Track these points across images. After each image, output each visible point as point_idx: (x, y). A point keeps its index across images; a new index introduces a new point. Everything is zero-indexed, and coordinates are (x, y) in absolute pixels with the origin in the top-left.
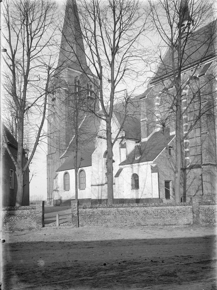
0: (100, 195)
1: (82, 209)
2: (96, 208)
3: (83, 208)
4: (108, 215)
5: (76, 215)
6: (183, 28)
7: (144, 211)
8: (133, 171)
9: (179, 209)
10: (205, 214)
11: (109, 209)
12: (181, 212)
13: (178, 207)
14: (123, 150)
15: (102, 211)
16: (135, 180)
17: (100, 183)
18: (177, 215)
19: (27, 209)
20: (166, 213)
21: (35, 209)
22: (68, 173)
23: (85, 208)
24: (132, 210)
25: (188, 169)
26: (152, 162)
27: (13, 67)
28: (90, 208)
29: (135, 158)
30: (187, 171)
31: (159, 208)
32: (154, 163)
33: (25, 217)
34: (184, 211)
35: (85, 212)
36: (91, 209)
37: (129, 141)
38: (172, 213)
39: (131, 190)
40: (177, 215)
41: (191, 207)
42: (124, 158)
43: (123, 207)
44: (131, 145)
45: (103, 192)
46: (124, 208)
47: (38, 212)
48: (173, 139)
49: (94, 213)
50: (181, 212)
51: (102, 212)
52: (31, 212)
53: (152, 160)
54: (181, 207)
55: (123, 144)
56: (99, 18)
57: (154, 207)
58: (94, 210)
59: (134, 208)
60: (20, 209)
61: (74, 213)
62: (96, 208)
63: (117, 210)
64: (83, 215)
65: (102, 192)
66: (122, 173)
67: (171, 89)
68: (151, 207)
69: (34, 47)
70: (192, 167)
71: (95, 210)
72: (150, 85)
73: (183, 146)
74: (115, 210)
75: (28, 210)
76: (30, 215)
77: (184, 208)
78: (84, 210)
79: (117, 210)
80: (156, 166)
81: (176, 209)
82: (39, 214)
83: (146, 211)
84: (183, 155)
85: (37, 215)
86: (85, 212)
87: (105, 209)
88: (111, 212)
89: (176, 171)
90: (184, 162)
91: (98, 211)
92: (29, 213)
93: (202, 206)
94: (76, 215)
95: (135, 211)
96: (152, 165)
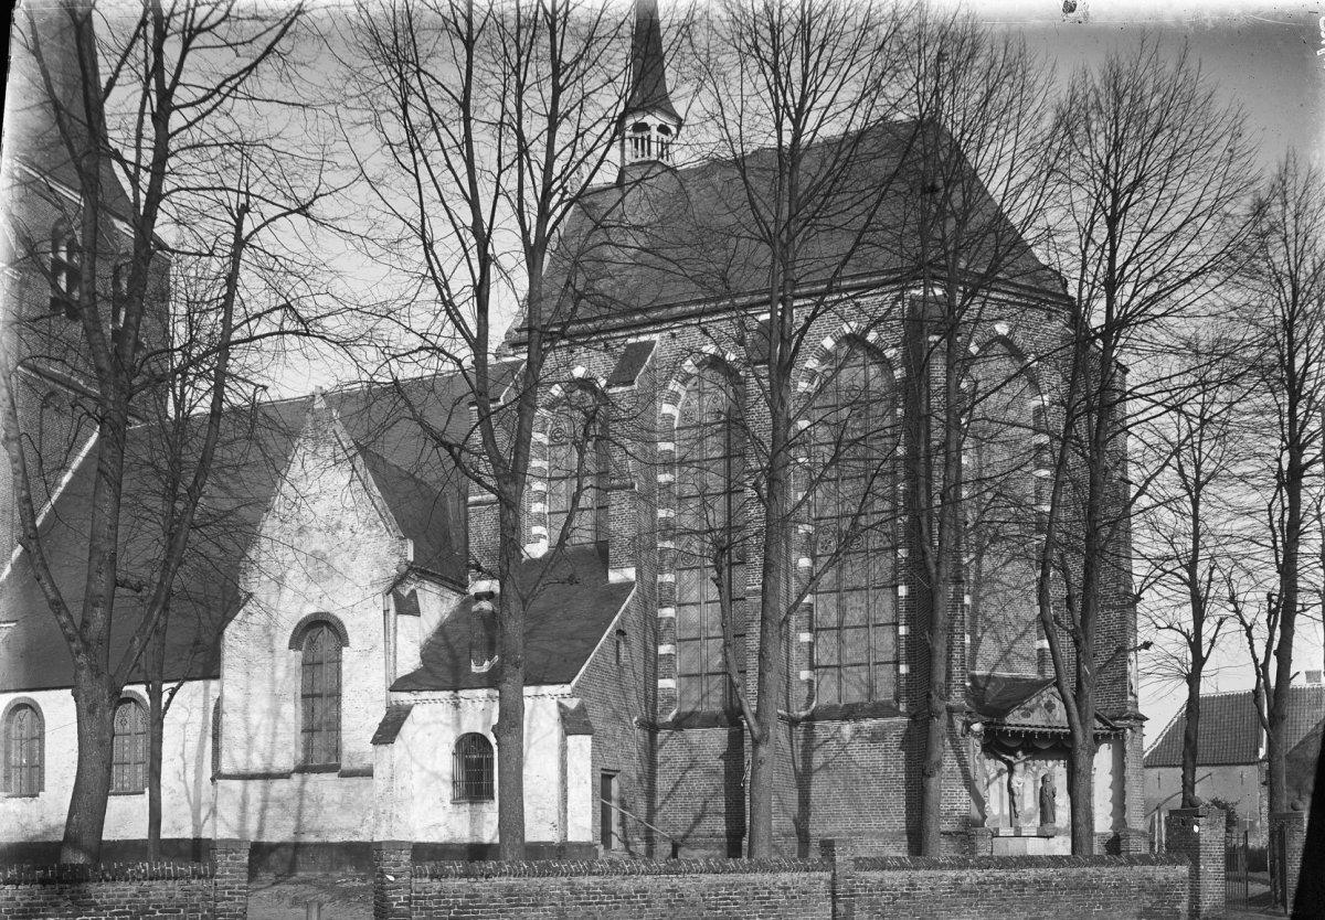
0: (252, 826)
3: (432, 877)
7: (668, 891)
8: (458, 722)
9: (789, 884)
10: (871, 903)
11: (540, 881)
13: (785, 877)
14: (406, 621)
15: (510, 889)
16: (467, 760)
17: (257, 765)
21: (212, 877)
22: (37, 705)
23: (439, 877)
24: (625, 885)
25: (665, 726)
26: (567, 689)
28: (461, 876)
31: (722, 878)
33: (158, 914)
36: (464, 881)
39: (449, 806)
41: (827, 876)
44: (436, 605)
45: (270, 813)
46: (597, 879)
53: (569, 683)
54: (795, 875)
61: (394, 899)
64: (431, 909)
65: (264, 809)
66: (407, 728)
67: (621, 389)
69: (562, 146)
70: (681, 723)
71: (480, 885)
74: (563, 884)
75: (170, 883)
76: (182, 906)
78: (436, 884)
80: (582, 709)
81: (779, 883)
82: (230, 899)
83: (676, 891)
84: (654, 667)
85: (220, 906)
86: (441, 895)
87: (521, 880)
88: (546, 893)
89: (762, 736)
90: (651, 697)
92: (178, 895)
93: (862, 874)
95: (636, 892)
96: (563, 701)
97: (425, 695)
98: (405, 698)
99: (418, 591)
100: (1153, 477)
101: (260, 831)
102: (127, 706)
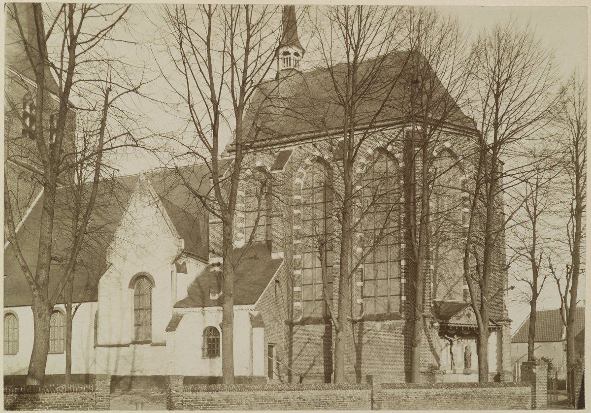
2: (217, 392)
3: (192, 391)
4: (237, 404)
5: (179, 404)
6: (288, 58)
7: (298, 398)
9: (352, 395)
11: (241, 393)
12: (355, 401)
13: (350, 392)
18: (349, 405)
19: (75, 392)
20: (333, 402)
23: (195, 391)
24: (279, 395)
25: (297, 324)
26: (253, 307)
31: (322, 392)
32: (255, 310)
35: (196, 398)
36: (207, 393)
37: (191, 260)
38: (342, 401)
40: (349, 405)
41: (369, 391)
43: (265, 390)
46: (266, 392)
47: (102, 399)
48: (280, 267)
50: (355, 401)
51: (227, 399)
52: (84, 399)
53: (254, 304)
57: (315, 391)
58: (212, 395)
59: (283, 391)
60: (59, 392)
61: (175, 401)
62: (217, 392)
63: (254, 395)
64: (192, 406)
67: (277, 171)
68: (310, 391)
70: (304, 322)
72: (228, 154)
75: (75, 394)
76: (80, 404)
78: (194, 395)
79: (254, 395)
80: (260, 316)
82: (102, 401)
89: (340, 328)
91: (221, 398)
92: (79, 399)
94: (179, 404)
95: (284, 399)
96: (251, 312)
98: (180, 311)
99: (187, 263)
100: (515, 212)
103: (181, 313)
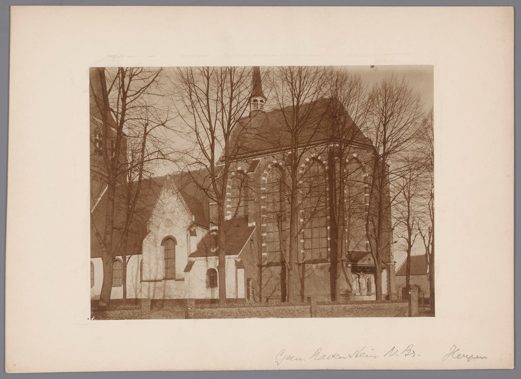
1: (200, 309)
4: (229, 316)
5: (193, 316)
7: (266, 311)
9: (299, 309)
11: (230, 309)
12: (300, 313)
13: (297, 307)
17: (153, 278)
19: (129, 309)
24: (254, 310)
26: (237, 256)
27: (200, 145)
28: (209, 308)
29: (211, 250)
30: (263, 269)
34: (303, 311)
36: (210, 309)
38: (293, 313)
41: (309, 307)
42: (194, 249)
44: (201, 233)
46: (246, 308)
49: (213, 313)
50: (300, 313)
53: (238, 254)
54: (300, 307)
55: (193, 230)
56: (222, 87)
61: (190, 315)
63: (238, 310)
67: (251, 173)
70: (268, 265)
73: (261, 240)
74: (237, 310)
75: (129, 311)
76: (132, 317)
77: (303, 308)
78: (202, 310)
79: (238, 310)
80: (241, 261)
81: (296, 309)
82: (145, 315)
90: (260, 258)
96: (236, 259)
97: (198, 258)
98: (193, 259)
99: (196, 229)
101: (154, 296)
102: (117, 262)
103: (193, 260)
